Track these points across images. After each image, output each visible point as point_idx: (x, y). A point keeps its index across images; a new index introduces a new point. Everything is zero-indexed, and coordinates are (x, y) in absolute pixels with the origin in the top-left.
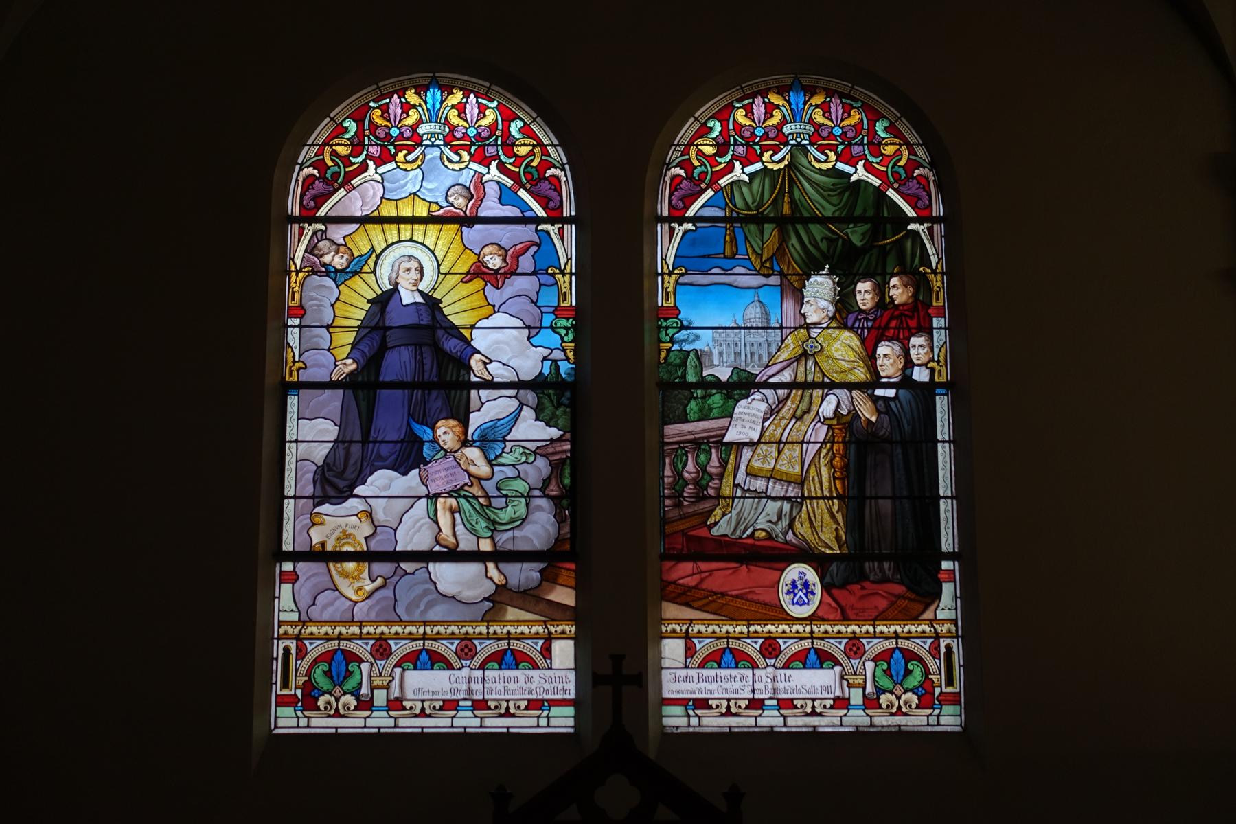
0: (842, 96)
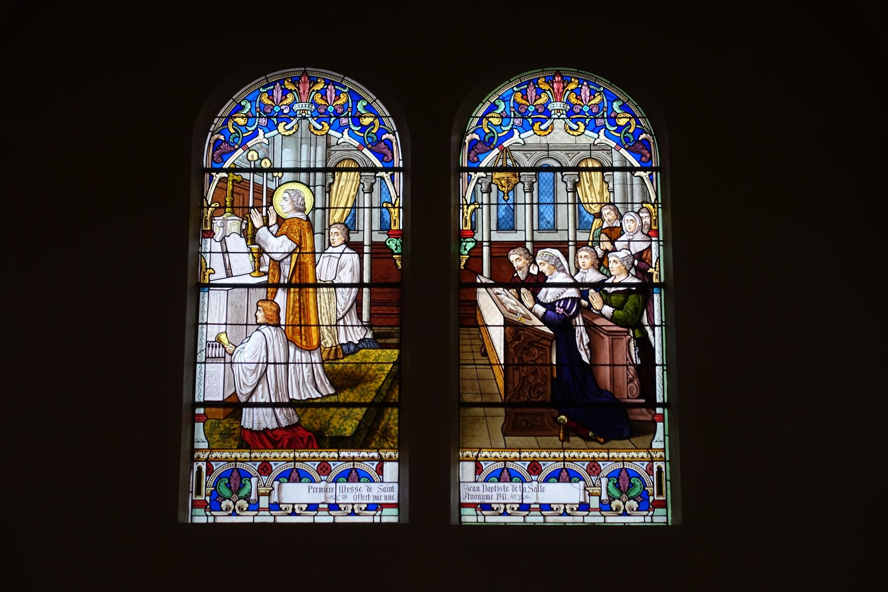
0: (334, 84)
